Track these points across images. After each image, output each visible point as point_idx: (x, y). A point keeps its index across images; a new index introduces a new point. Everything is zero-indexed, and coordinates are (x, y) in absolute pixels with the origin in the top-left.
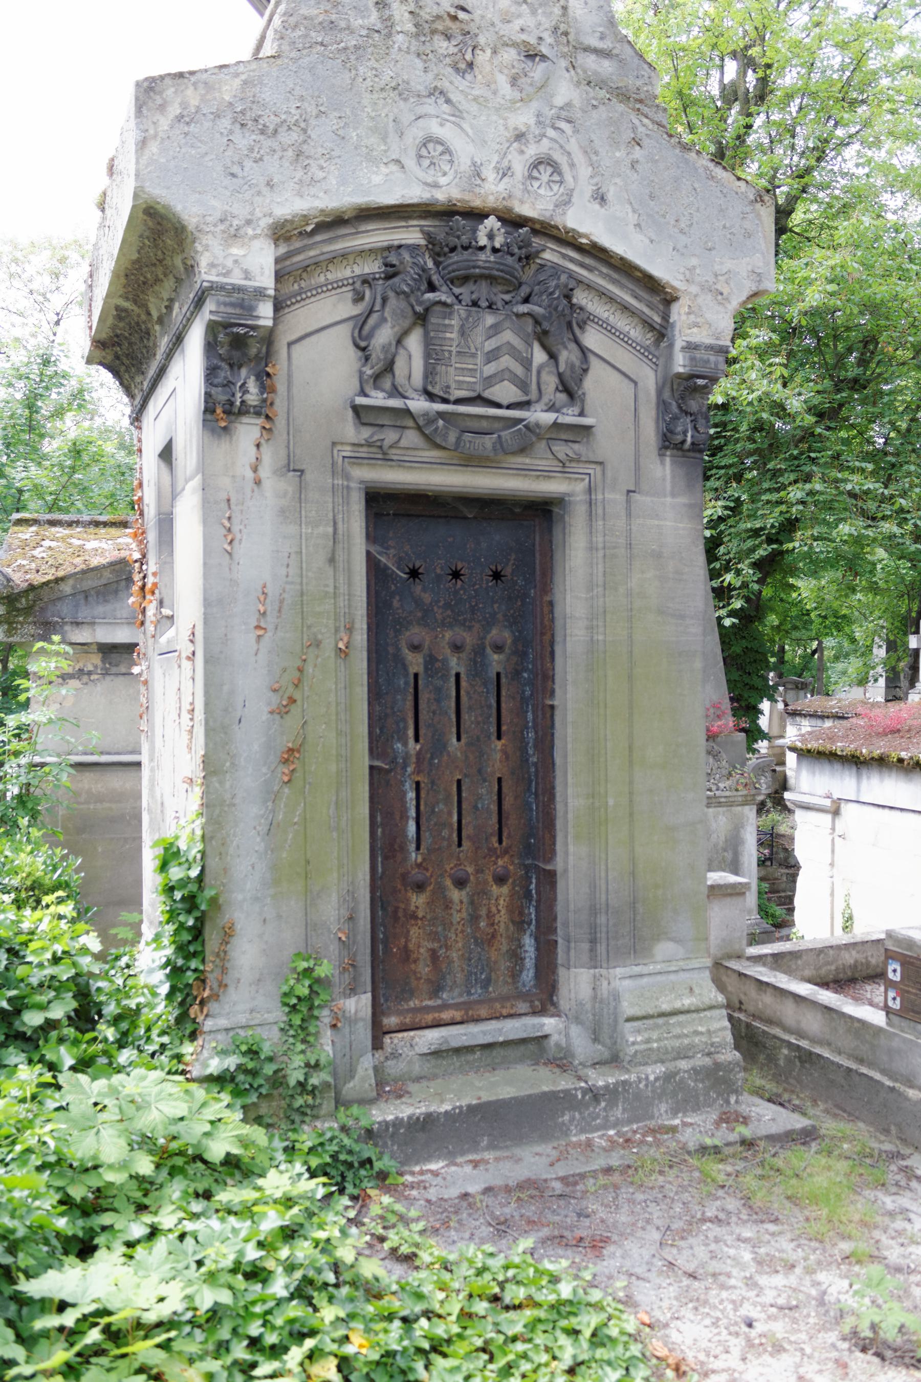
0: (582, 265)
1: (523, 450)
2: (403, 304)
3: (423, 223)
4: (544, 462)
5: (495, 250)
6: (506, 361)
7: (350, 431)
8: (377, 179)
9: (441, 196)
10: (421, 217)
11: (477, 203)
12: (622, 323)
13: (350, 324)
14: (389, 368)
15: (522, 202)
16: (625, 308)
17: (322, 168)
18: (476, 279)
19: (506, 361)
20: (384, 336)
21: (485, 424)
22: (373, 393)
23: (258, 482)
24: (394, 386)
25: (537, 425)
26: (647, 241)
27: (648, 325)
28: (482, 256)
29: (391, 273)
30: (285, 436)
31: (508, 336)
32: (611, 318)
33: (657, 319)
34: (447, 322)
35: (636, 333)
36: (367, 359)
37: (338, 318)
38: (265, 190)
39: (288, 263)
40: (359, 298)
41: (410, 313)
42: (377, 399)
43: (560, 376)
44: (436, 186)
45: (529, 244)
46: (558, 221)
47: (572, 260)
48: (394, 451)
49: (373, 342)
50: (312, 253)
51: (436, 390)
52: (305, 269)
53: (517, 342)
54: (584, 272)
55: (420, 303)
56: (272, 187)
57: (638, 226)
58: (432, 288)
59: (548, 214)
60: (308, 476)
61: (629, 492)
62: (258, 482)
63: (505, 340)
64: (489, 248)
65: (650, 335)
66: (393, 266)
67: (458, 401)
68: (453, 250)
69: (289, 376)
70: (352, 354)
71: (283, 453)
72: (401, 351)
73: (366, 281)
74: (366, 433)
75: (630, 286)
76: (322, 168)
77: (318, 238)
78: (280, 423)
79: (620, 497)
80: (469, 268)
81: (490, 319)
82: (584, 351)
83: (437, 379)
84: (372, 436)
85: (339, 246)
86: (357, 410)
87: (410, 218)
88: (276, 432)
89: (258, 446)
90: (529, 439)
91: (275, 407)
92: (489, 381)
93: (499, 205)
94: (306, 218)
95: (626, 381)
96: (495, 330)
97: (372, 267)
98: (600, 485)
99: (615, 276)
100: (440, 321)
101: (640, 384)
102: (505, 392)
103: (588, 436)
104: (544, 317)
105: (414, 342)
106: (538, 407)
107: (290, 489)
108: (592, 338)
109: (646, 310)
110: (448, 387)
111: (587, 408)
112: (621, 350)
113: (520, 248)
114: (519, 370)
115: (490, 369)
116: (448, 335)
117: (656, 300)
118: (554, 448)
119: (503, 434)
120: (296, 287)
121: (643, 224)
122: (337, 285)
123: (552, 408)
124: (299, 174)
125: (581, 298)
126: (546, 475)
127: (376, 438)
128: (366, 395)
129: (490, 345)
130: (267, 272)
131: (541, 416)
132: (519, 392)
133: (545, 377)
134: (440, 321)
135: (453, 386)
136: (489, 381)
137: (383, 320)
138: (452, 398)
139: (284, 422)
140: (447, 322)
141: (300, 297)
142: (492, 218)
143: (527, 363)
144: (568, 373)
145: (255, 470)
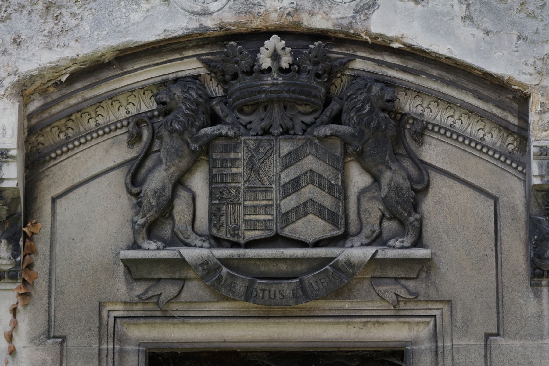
0: (404, 70)
1: (337, 293)
2: (178, 142)
3: (199, 52)
4: (369, 306)
5: (281, 70)
6: (309, 192)
7: (120, 287)
8: (136, 17)
9: (210, 23)
10: (197, 46)
11: (257, 24)
12: (473, 128)
13: (125, 169)
14: (166, 211)
15: (312, 14)
16: (471, 111)
17: (74, 15)
18: (266, 106)
19: (309, 192)
20: (157, 179)
21: (283, 267)
22: (146, 244)
23: (12, 352)
24: (174, 233)
25: (349, 263)
26: (481, 34)
27: (503, 127)
28: (269, 80)
29: (165, 109)
30: (45, 300)
31: (310, 163)
32: (458, 124)
33: (513, 120)
34: (232, 156)
35: (492, 137)
36: (139, 204)
37: (111, 164)
38: (11, 48)
39: (46, 115)
40: (134, 139)
41: (187, 152)
42: (151, 250)
43: (384, 200)
44: (206, 13)
45: (325, 58)
46: (359, 27)
47: (390, 66)
48: (174, 306)
49: (145, 187)
50: (73, 101)
51: (222, 234)
52: (69, 117)
53: (321, 168)
54: (410, 78)
55: (196, 140)
56: (19, 44)
57: (468, 18)
58: (215, 120)
59: (345, 22)
60: (70, 343)
61: (487, 336)
62: (12, 352)
63: (306, 168)
64: (274, 69)
65: (510, 139)
66: (164, 103)
67: (251, 244)
68: (235, 76)
69: (53, 233)
70: (125, 201)
71: (42, 318)
72: (183, 194)
73: (138, 121)
74: (139, 289)
75: (470, 86)
76: (74, 15)
77: (78, 86)
78: (40, 287)
79: (477, 344)
80: (252, 94)
81: (286, 148)
82: (423, 167)
83: (223, 220)
84: (146, 292)
85: (103, 89)
86: (128, 264)
87: (185, 48)
88: (35, 296)
89: (14, 311)
90: (340, 281)
91: (35, 269)
92: (289, 217)
93: (286, 21)
94: (56, 69)
95: (482, 197)
96: (293, 158)
97: (146, 105)
98: (448, 328)
99: (450, 77)
100: (224, 156)
101: (503, 200)
102: (312, 227)
103: (429, 269)
104: (353, 136)
105: (199, 182)
106: (357, 241)
107: (49, 359)
108: (433, 152)
109: (497, 111)
110: (237, 228)
111: (426, 235)
112: (474, 161)
113: (316, 64)
114: (327, 200)
115: (289, 203)
116: (235, 170)
117: (507, 98)
118: (377, 289)
119: (305, 278)
120: (93, 123)
121: (475, 15)
122: (112, 127)
123: (378, 240)
124: (50, 24)
125: (409, 105)
126: (376, 318)
127: (150, 293)
128: (139, 248)
129: (287, 176)
130: (9, 132)
131: (358, 253)
132: (328, 226)
133: (365, 204)
134: (224, 156)
135: (243, 227)
136: (289, 217)
137: (159, 162)
138: (242, 241)
139: (45, 284)
140: (232, 156)
141: (66, 146)
142: (275, 38)
143: (341, 192)
144: (393, 195)
145: (10, 338)
